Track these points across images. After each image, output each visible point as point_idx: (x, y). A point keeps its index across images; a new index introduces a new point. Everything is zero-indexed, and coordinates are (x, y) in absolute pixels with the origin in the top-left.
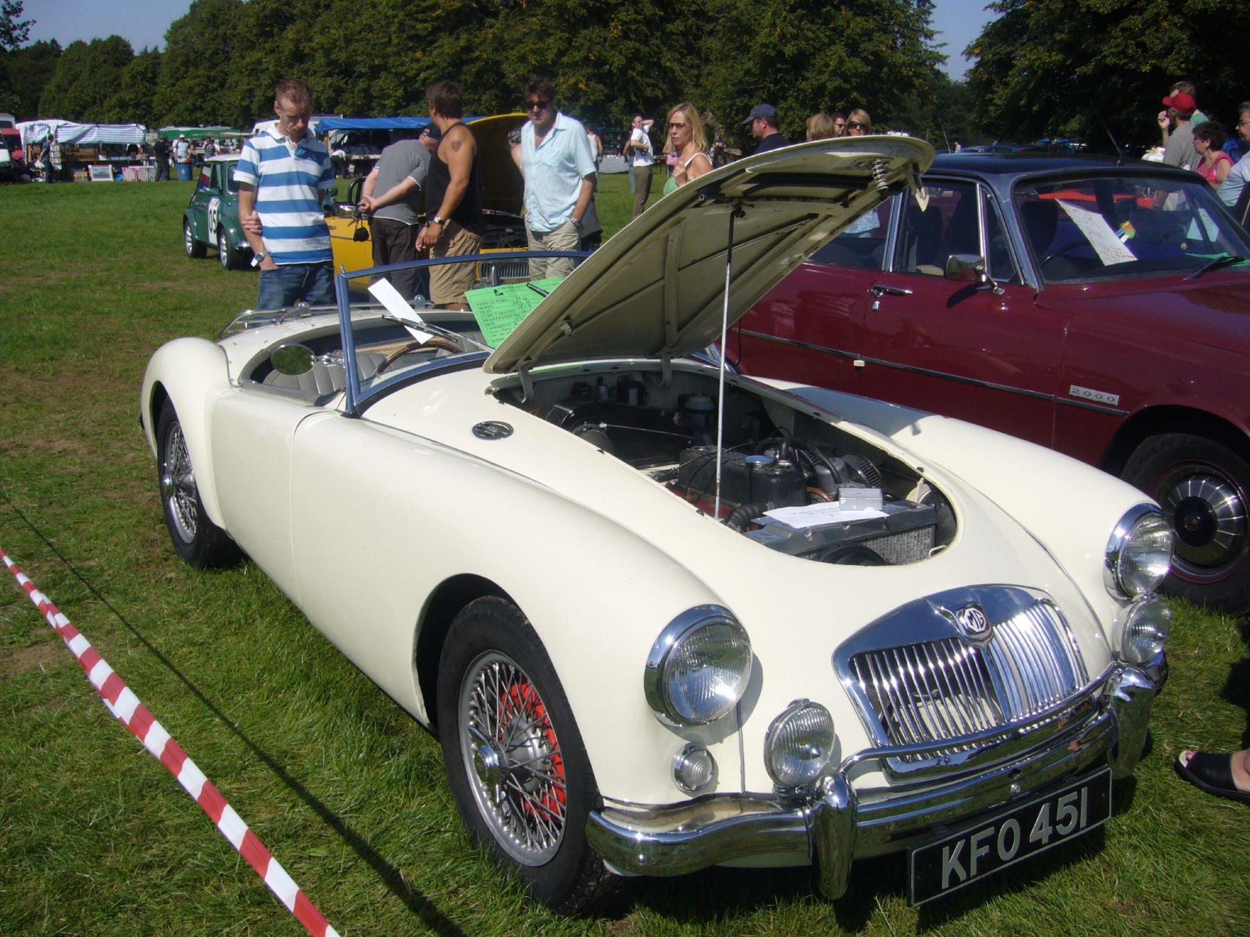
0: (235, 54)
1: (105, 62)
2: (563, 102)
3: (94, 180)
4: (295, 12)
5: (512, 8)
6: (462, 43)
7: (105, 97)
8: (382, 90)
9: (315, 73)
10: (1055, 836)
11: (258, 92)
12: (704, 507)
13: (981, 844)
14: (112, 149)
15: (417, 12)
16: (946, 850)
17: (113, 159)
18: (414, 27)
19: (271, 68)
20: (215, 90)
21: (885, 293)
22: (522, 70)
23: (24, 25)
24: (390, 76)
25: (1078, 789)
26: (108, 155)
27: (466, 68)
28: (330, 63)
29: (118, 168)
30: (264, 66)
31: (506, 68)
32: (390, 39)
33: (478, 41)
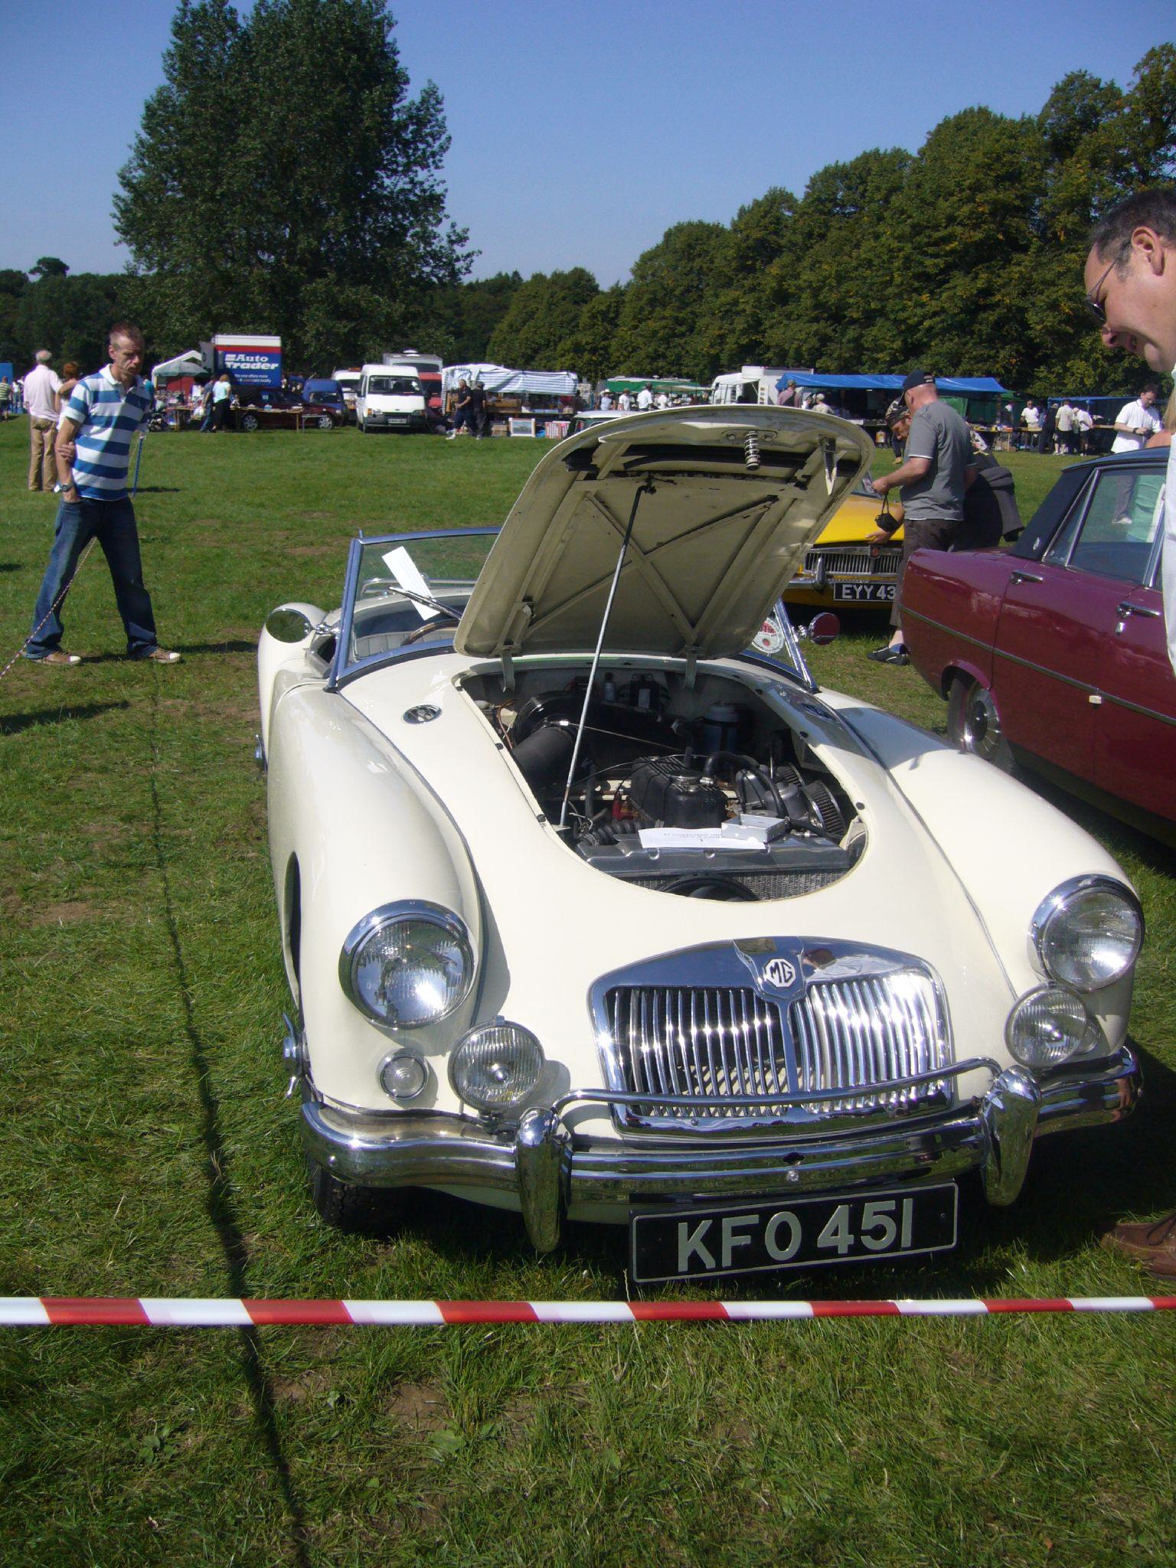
0: (708, 292)
1: (564, 298)
2: (1101, 362)
3: (513, 435)
4: (783, 242)
5: (1048, 241)
6: (980, 284)
7: (560, 338)
8: (875, 340)
9: (799, 316)
10: (857, 1248)
11: (731, 340)
12: (550, 813)
13: (737, 1231)
14: (539, 400)
15: (929, 244)
16: (683, 1227)
17: (537, 411)
18: (921, 263)
19: (749, 309)
20: (683, 335)
21: (1134, 612)
22: (1051, 320)
23: (469, 255)
24: (888, 324)
25: (898, 1199)
26: (532, 406)
27: (982, 315)
28: (816, 307)
29: (541, 422)
30: (741, 307)
31: (1031, 317)
32: (892, 277)
33: (1000, 281)
